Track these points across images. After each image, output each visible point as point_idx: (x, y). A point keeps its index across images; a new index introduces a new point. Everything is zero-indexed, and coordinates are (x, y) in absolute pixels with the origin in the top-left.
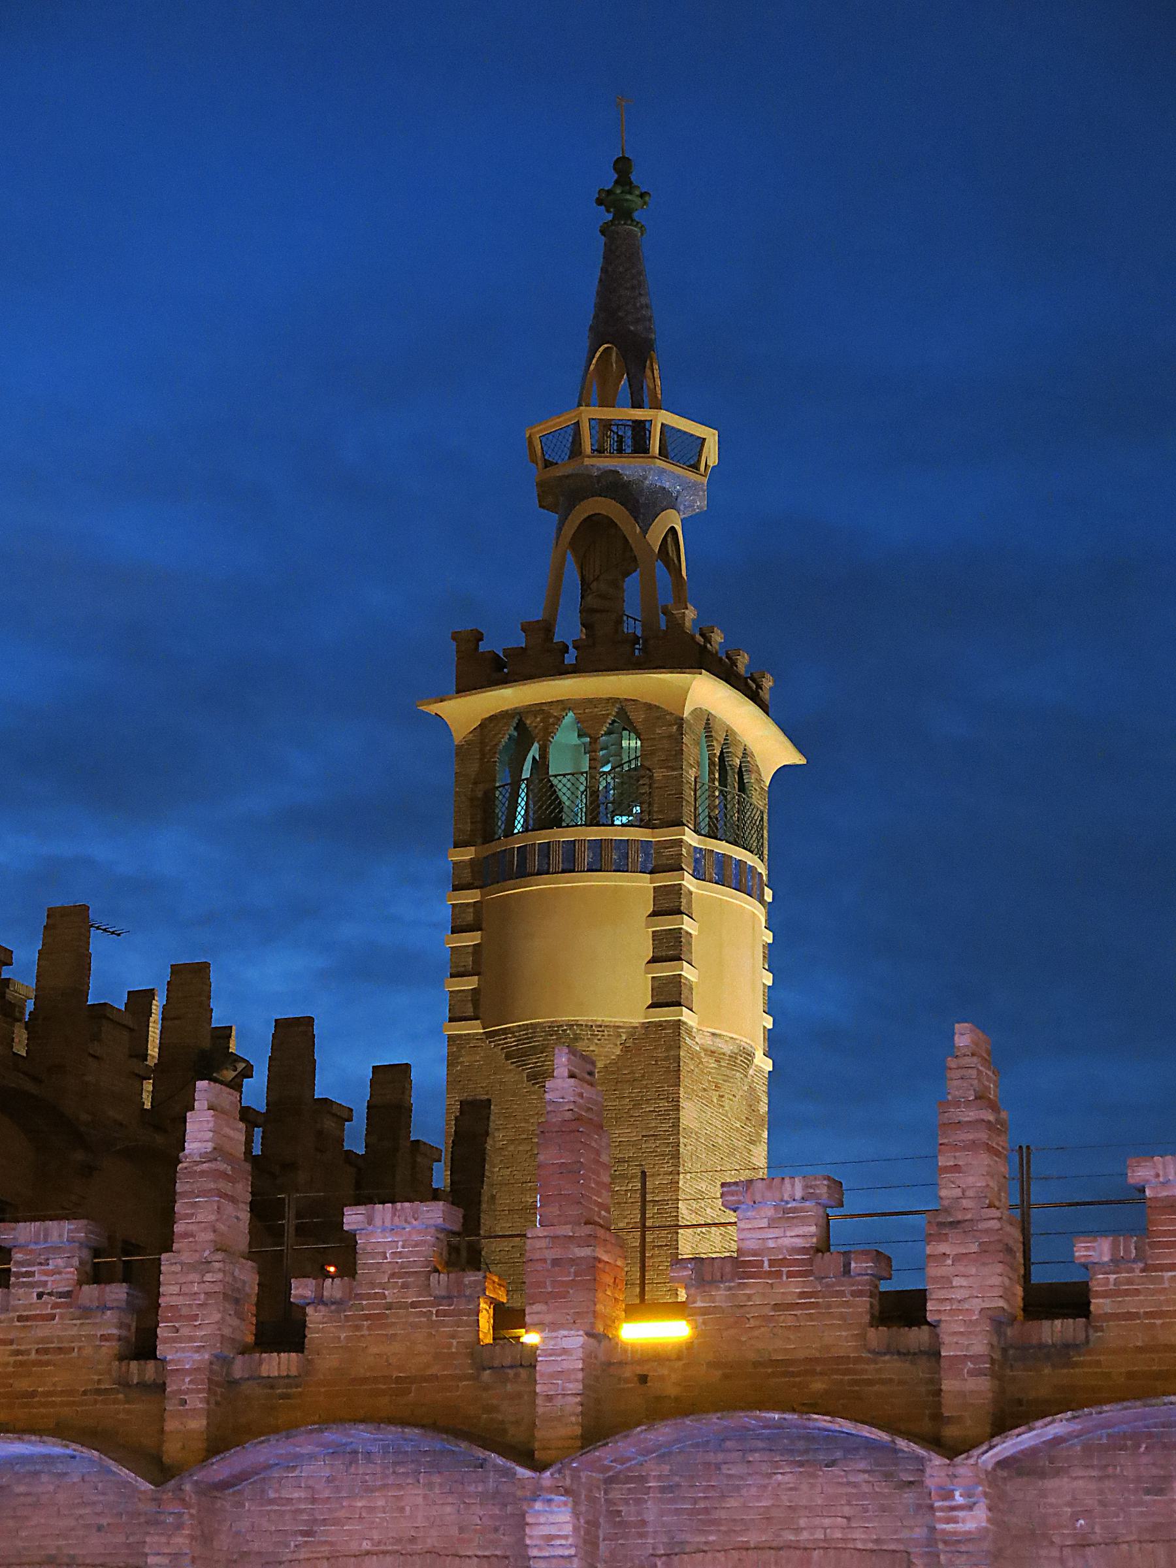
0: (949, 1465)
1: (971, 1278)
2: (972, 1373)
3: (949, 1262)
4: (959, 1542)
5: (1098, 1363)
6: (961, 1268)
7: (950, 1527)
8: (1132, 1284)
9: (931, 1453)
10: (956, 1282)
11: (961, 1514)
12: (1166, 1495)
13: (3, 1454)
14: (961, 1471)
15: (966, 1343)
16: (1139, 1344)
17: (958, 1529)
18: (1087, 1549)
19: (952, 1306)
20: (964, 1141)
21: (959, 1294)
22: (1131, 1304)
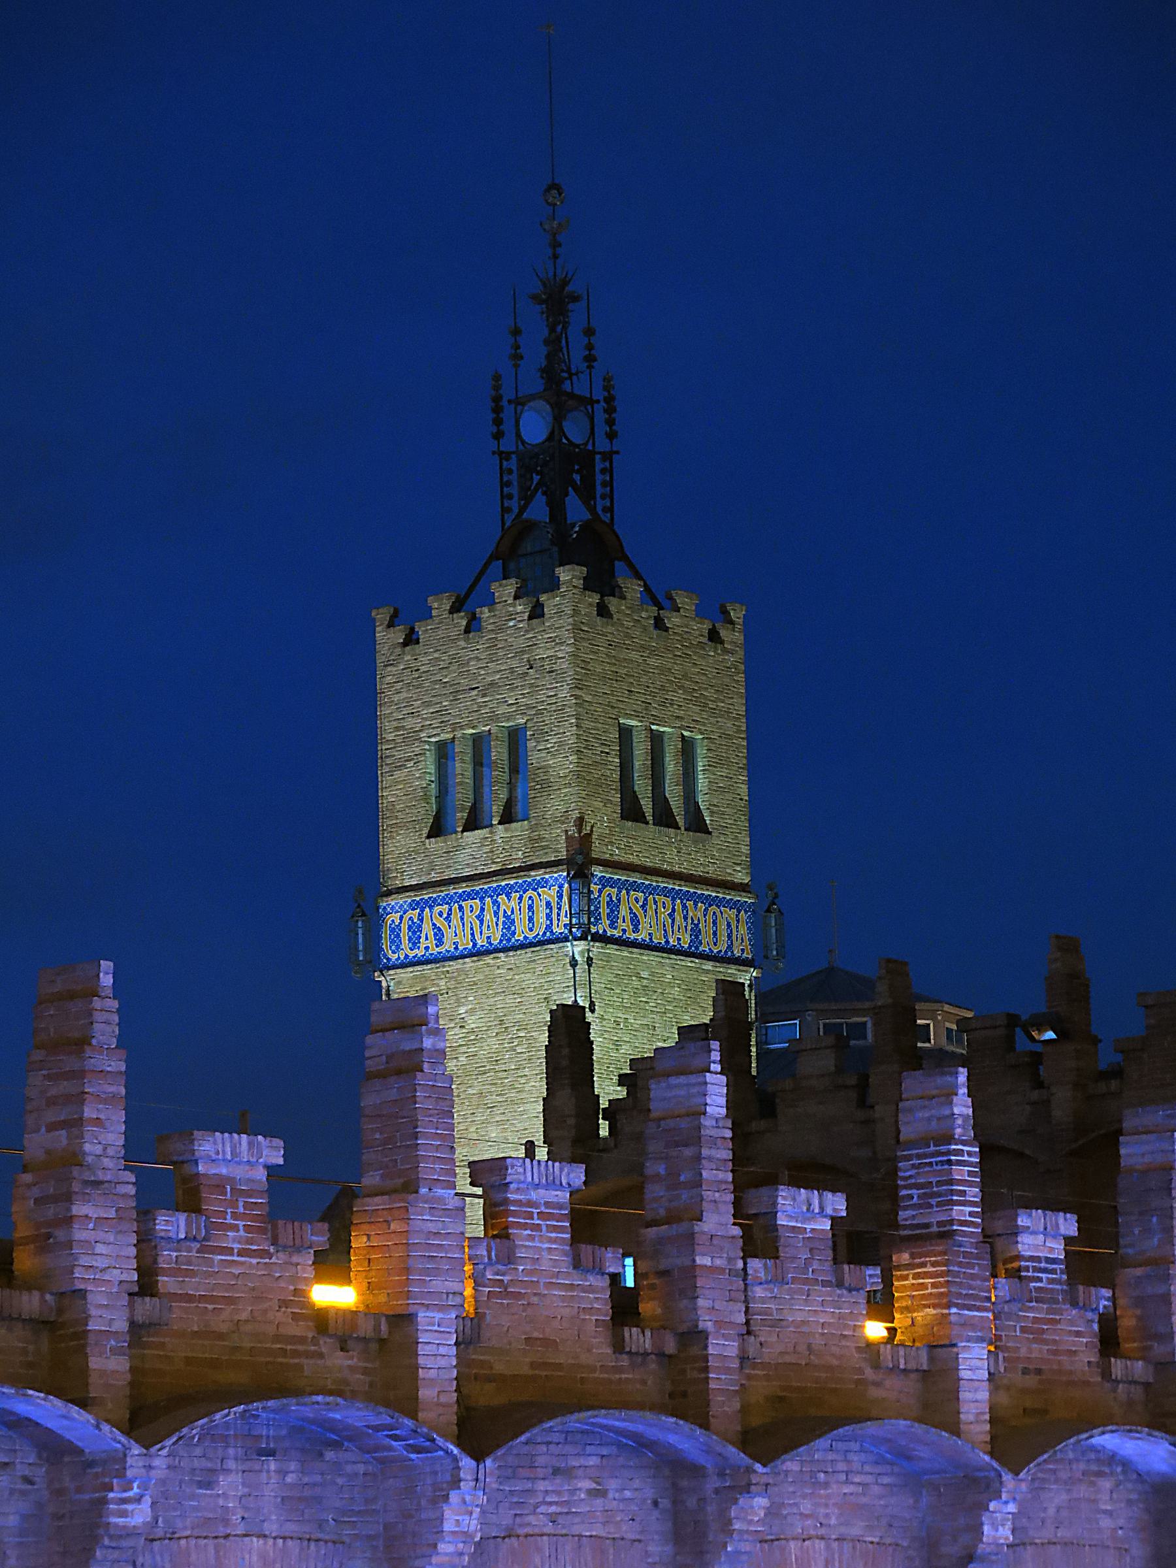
0: (145, 1455)
1: (110, 1246)
2: (115, 1351)
3: (91, 1226)
4: (121, 1536)
5: (162, 1345)
6: (100, 1235)
7: (120, 1521)
8: (190, 1265)
9: (132, 1441)
10: (100, 1248)
11: (129, 1507)
12: (212, 1489)
13: (1139, 1550)
14: (156, 1462)
15: (109, 1317)
16: (196, 1329)
17: (128, 1524)
18: (155, 1543)
19: (95, 1275)
20: (106, 1093)
21: (99, 1263)
22: (192, 1286)
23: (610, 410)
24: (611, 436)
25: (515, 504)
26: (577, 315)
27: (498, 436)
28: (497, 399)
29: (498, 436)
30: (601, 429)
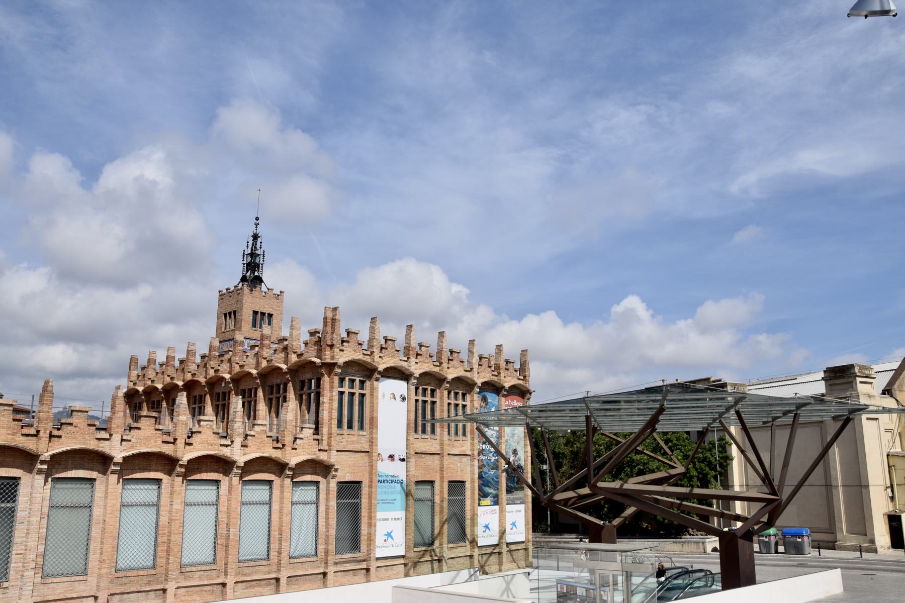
23: (264, 256)
24: (263, 261)
25: (245, 273)
26: (259, 240)
27: (243, 260)
28: (244, 254)
29: (243, 260)
30: (262, 259)
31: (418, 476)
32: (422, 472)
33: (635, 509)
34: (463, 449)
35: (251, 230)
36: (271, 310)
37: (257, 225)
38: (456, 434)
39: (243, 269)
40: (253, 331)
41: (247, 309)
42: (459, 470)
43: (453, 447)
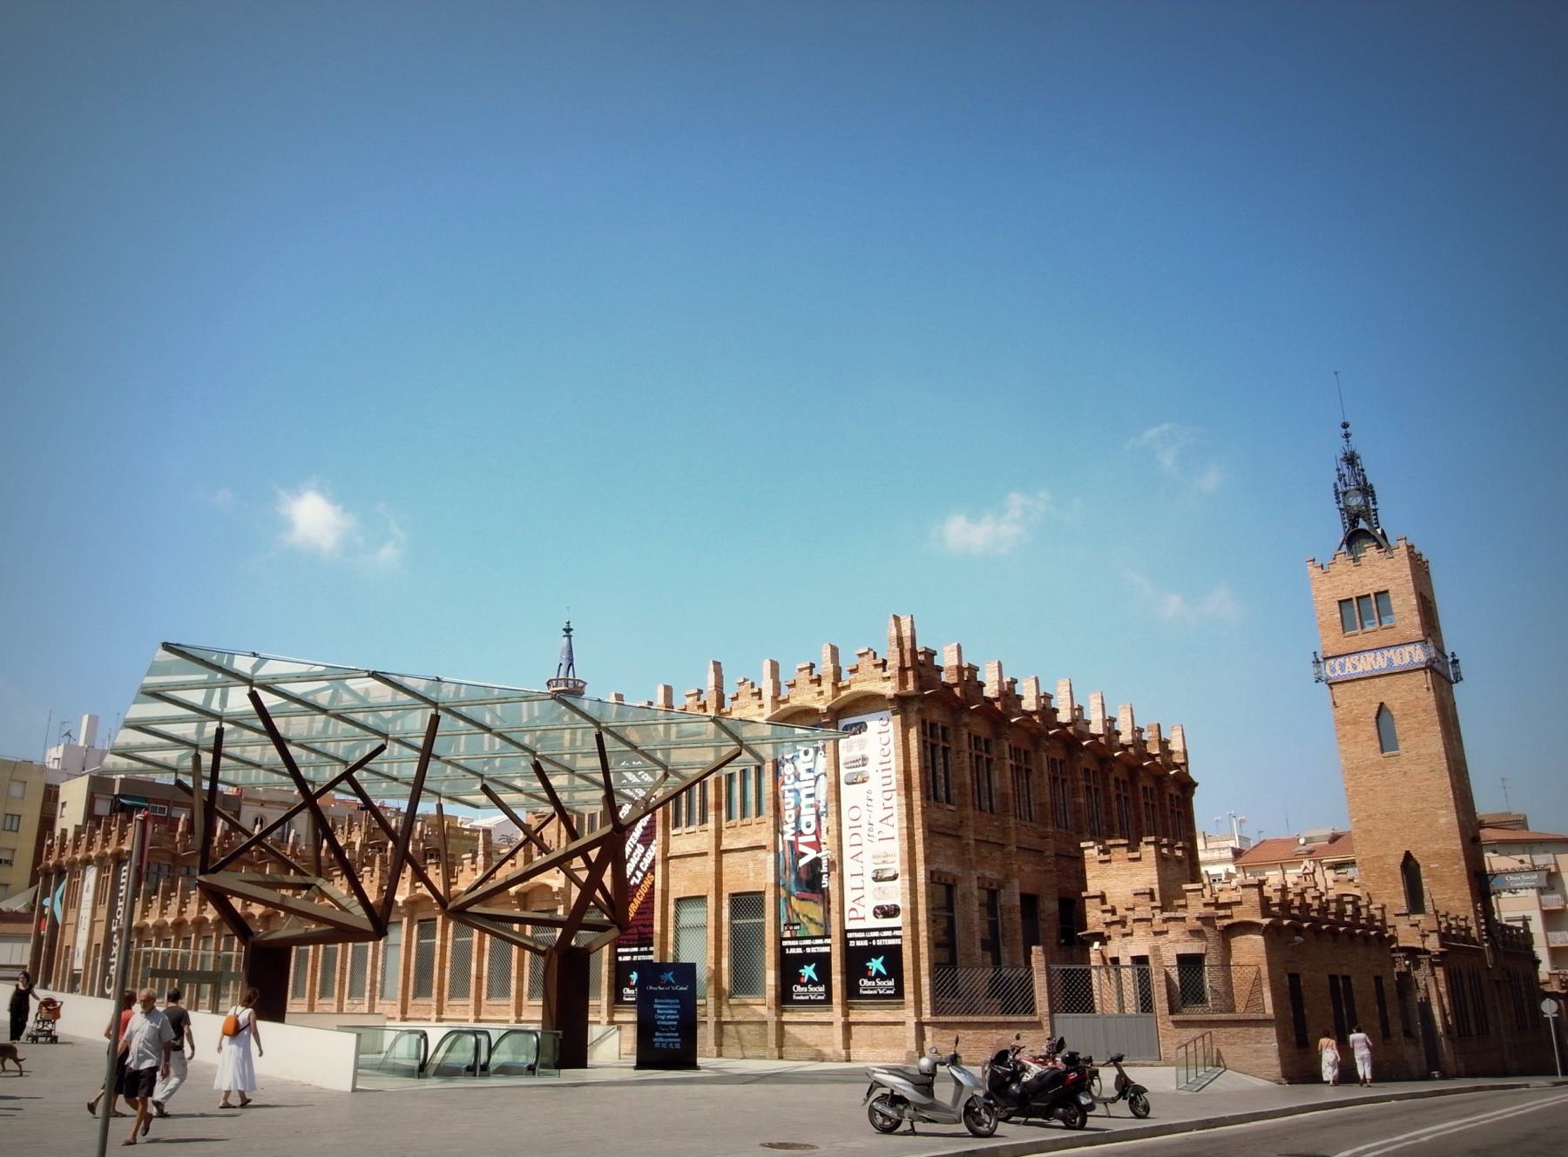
31: (679, 890)
32: (686, 883)
33: (598, 891)
34: (757, 837)
35: (1338, 448)
36: (1381, 583)
37: (1347, 436)
38: (743, 815)
39: (1376, 519)
40: (1348, 639)
41: (1326, 603)
42: (752, 874)
43: (739, 837)
